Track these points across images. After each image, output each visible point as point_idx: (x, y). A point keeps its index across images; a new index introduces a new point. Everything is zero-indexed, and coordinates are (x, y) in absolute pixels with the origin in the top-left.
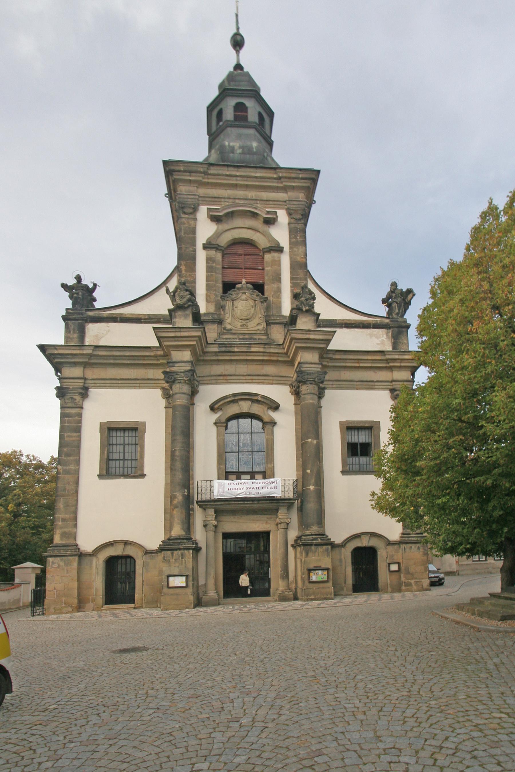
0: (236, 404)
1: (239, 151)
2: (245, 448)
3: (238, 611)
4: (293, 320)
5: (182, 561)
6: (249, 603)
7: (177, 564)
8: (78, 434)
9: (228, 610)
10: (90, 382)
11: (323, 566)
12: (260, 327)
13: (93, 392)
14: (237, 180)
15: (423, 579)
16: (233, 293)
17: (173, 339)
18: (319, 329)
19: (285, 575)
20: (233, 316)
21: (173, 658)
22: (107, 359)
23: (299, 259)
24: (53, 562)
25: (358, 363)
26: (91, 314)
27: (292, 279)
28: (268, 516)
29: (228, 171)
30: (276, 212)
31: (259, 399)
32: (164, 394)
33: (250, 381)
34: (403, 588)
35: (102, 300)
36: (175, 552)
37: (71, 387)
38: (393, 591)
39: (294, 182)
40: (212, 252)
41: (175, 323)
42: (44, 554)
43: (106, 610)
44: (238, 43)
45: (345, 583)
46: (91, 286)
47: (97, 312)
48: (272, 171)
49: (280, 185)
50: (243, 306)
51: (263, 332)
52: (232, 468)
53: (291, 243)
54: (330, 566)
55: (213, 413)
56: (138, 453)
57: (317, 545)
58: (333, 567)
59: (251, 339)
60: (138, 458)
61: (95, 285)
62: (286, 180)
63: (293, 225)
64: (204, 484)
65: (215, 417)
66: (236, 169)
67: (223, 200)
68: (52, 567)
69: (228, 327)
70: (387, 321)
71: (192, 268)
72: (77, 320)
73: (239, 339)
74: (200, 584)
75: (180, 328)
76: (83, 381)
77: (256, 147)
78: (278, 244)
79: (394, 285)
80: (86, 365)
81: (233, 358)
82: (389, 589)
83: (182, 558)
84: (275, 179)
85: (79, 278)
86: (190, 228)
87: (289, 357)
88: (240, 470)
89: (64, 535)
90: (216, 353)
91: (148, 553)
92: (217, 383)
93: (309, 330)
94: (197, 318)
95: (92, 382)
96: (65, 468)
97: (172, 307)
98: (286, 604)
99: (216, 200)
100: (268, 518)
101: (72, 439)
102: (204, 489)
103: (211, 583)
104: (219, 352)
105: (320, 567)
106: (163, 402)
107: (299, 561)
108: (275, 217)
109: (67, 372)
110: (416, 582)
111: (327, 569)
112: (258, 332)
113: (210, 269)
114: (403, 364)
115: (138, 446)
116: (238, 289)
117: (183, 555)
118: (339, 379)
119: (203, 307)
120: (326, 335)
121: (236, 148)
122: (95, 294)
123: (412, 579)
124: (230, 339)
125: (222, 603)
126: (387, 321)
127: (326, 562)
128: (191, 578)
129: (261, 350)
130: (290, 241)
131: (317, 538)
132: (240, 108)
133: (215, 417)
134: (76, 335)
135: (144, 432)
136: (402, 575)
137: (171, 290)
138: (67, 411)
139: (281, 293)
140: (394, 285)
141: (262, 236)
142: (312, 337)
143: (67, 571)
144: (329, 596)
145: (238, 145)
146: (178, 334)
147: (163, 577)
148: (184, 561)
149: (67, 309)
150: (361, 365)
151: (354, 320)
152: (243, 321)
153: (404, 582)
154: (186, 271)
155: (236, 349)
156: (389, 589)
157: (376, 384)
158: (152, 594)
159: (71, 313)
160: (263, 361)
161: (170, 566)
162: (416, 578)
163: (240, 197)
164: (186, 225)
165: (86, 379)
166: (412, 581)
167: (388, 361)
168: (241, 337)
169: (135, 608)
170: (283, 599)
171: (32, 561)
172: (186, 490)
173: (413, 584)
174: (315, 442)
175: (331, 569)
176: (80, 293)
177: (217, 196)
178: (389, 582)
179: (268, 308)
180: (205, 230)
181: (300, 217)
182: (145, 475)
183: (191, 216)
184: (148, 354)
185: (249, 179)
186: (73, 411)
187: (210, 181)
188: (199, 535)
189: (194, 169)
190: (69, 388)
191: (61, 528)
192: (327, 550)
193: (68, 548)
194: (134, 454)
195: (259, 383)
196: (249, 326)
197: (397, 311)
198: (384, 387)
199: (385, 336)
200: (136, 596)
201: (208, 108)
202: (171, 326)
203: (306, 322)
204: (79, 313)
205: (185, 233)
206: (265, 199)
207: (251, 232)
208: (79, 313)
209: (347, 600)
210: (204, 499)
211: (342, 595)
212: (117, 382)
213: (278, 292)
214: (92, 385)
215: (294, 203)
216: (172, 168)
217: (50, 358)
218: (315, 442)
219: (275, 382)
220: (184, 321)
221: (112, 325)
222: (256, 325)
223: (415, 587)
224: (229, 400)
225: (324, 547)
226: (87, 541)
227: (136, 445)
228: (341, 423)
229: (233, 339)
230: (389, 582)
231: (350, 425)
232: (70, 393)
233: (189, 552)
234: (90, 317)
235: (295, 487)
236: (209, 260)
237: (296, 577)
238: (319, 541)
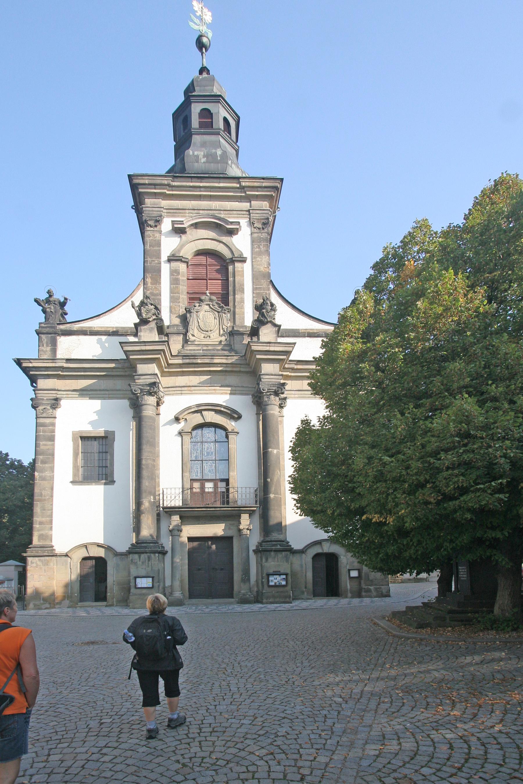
1: (204, 160)
2: (209, 457)
3: (199, 612)
4: (254, 332)
5: (148, 563)
6: (212, 604)
7: (144, 567)
8: (52, 442)
9: (191, 611)
11: (282, 572)
14: (201, 191)
15: (382, 585)
17: (138, 353)
18: (280, 340)
21: (122, 650)
23: (262, 269)
24: (31, 562)
26: (62, 327)
27: (254, 289)
29: (192, 182)
30: (239, 223)
32: (132, 405)
33: (214, 391)
34: (363, 594)
36: (142, 556)
37: (45, 398)
38: (352, 597)
39: (257, 191)
41: (140, 336)
42: (25, 555)
43: (81, 607)
47: (68, 325)
52: (197, 476)
53: (252, 253)
54: (289, 571)
56: (108, 461)
57: (276, 551)
58: (291, 571)
60: (108, 465)
61: (49, 292)
62: (249, 189)
63: (255, 235)
64: (169, 491)
66: (199, 180)
68: (31, 567)
71: (157, 280)
72: (50, 333)
73: (203, 350)
74: (166, 585)
75: (145, 342)
77: (220, 155)
82: (349, 595)
83: (149, 561)
84: (238, 188)
85: (50, 293)
87: (251, 368)
88: (204, 478)
89: (41, 537)
90: (180, 365)
93: (269, 343)
94: (161, 330)
96: (41, 474)
97: (138, 321)
98: (246, 606)
99: (181, 211)
100: (230, 524)
101: (47, 447)
102: (169, 496)
103: (177, 584)
104: (183, 364)
105: (280, 572)
108: (238, 227)
110: (376, 589)
111: (286, 575)
113: (174, 281)
115: (108, 454)
117: (149, 558)
118: (301, 389)
119: (167, 318)
120: (286, 346)
121: (201, 157)
124: (194, 350)
125: (187, 603)
127: (285, 567)
128: (156, 580)
129: (224, 361)
132: (206, 114)
134: (49, 349)
136: (362, 582)
137: (137, 304)
138: (41, 420)
142: (272, 349)
143: (45, 570)
144: (288, 600)
145: (202, 154)
146: (144, 348)
147: (131, 578)
148: (150, 564)
149: (40, 323)
151: (316, 329)
153: (364, 588)
154: (152, 284)
155: (199, 361)
158: (122, 594)
159: (43, 327)
161: (137, 568)
162: (376, 585)
163: (204, 208)
164: (151, 238)
166: (372, 588)
168: (205, 348)
169: (106, 606)
170: (244, 601)
171: (14, 559)
172: (152, 497)
175: (290, 574)
176: (52, 307)
177: (181, 208)
180: (169, 244)
181: (265, 226)
182: (115, 481)
183: (156, 229)
185: (212, 190)
186: (47, 421)
189: (158, 182)
190: (43, 399)
191: (38, 531)
192: (286, 556)
193: (46, 549)
194: (104, 461)
201: (173, 115)
202: (136, 340)
204: (52, 327)
205: (150, 246)
206: (229, 209)
208: (52, 327)
209: (305, 604)
210: (169, 505)
211: (302, 599)
213: (241, 303)
215: (258, 212)
217: (26, 370)
219: (237, 392)
220: (149, 334)
221: (82, 338)
223: (374, 593)
224: (193, 410)
225: (283, 553)
226: (60, 545)
227: (106, 452)
229: (197, 350)
232: (43, 404)
233: (155, 555)
234: (62, 330)
236: (174, 273)
238: (279, 547)
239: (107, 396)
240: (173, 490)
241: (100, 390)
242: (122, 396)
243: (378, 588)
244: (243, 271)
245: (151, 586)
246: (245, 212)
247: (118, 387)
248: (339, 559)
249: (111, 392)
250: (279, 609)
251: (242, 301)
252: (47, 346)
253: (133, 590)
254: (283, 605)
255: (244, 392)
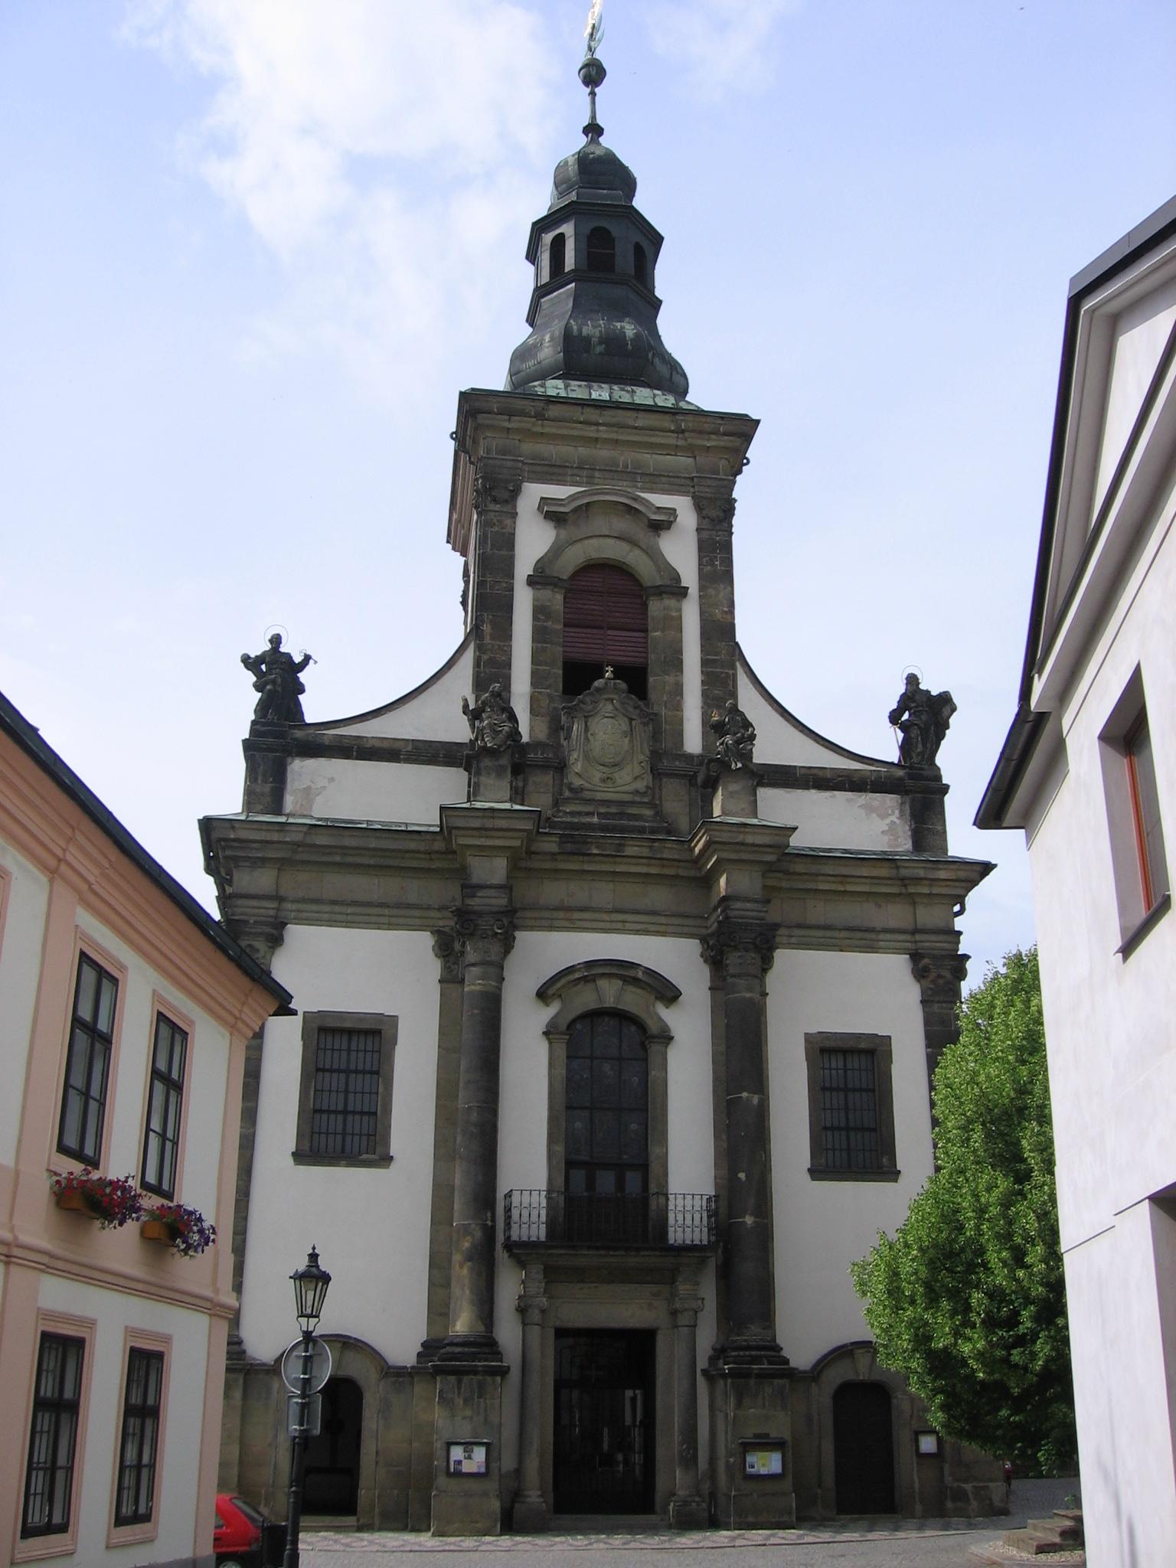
0: (591, 986)
10: (289, 906)
12: (640, 785)
13: (295, 933)
15: (991, 1480)
16: (588, 699)
19: (689, 1460)
20: (587, 757)
22: (329, 854)
25: (841, 883)
27: (705, 663)
28: (654, 1288)
31: (640, 975)
33: (619, 926)
34: (949, 1505)
35: (320, 703)
36: (466, 1379)
40: (546, 593)
44: (593, 74)
45: (820, 1486)
46: (298, 659)
48: (668, 417)
49: (681, 443)
50: (605, 731)
51: (646, 800)
53: (702, 576)
54: (787, 1436)
55: (541, 1004)
59: (621, 815)
61: (307, 659)
65: (547, 1013)
66: (598, 411)
67: (569, 471)
69: (577, 782)
70: (900, 773)
72: (272, 751)
76: (274, 905)
78: (677, 578)
79: (912, 680)
80: (283, 864)
81: (586, 867)
82: (919, 1508)
86: (503, 534)
91: (397, 1375)
92: (552, 928)
95: (295, 906)
99: (556, 470)
102: (525, 1213)
105: (767, 1436)
106: (434, 968)
107: (720, 1416)
109: (246, 880)
112: (637, 799)
113: (540, 634)
114: (935, 891)
116: (598, 690)
122: (302, 676)
123: (966, 1481)
124: (580, 813)
126: (900, 773)
127: (780, 1426)
130: (700, 570)
131: (761, 1357)
133: (547, 1013)
135: (394, 1041)
136: (947, 1468)
139: (682, 695)
140: (912, 680)
141: (644, 557)
142: (750, 839)
144: (785, 1518)
150: (849, 888)
152: (605, 769)
154: (493, 638)
156: (919, 1508)
157: (881, 936)
158: (395, 1492)
160: (647, 875)
161: (453, 1416)
164: (496, 529)
165: (280, 899)
166: (968, 1487)
167: (904, 881)
168: (602, 810)
173: (970, 1495)
174: (755, 1100)
178: (917, 1485)
179: (656, 736)
180: (533, 541)
184: (412, 846)
187: (546, 430)
188: (508, 1333)
190: (246, 922)
195: (637, 932)
196: (619, 782)
197: (920, 748)
198: (898, 945)
199: (897, 812)
200: (362, 1493)
203: (736, 792)
207: (625, 546)
212: (343, 909)
214: (293, 915)
216: (477, 404)
218: (755, 1100)
222: (630, 779)
224: (577, 975)
228: (809, 1038)
230: (917, 1485)
231: (828, 1044)
235: (713, 1214)
236: (540, 612)
237: (712, 1460)
239: (386, 920)
240: (689, 1201)
241: (369, 904)
242: (417, 921)
243: (982, 1488)
244: (680, 618)
245: (483, 1470)
246: (683, 481)
247: (412, 898)
248: (894, 1401)
249: (395, 912)
250: (772, 1541)
251: (678, 690)
252: (265, 781)
253: (442, 1481)
254: (781, 1533)
255: (685, 930)
